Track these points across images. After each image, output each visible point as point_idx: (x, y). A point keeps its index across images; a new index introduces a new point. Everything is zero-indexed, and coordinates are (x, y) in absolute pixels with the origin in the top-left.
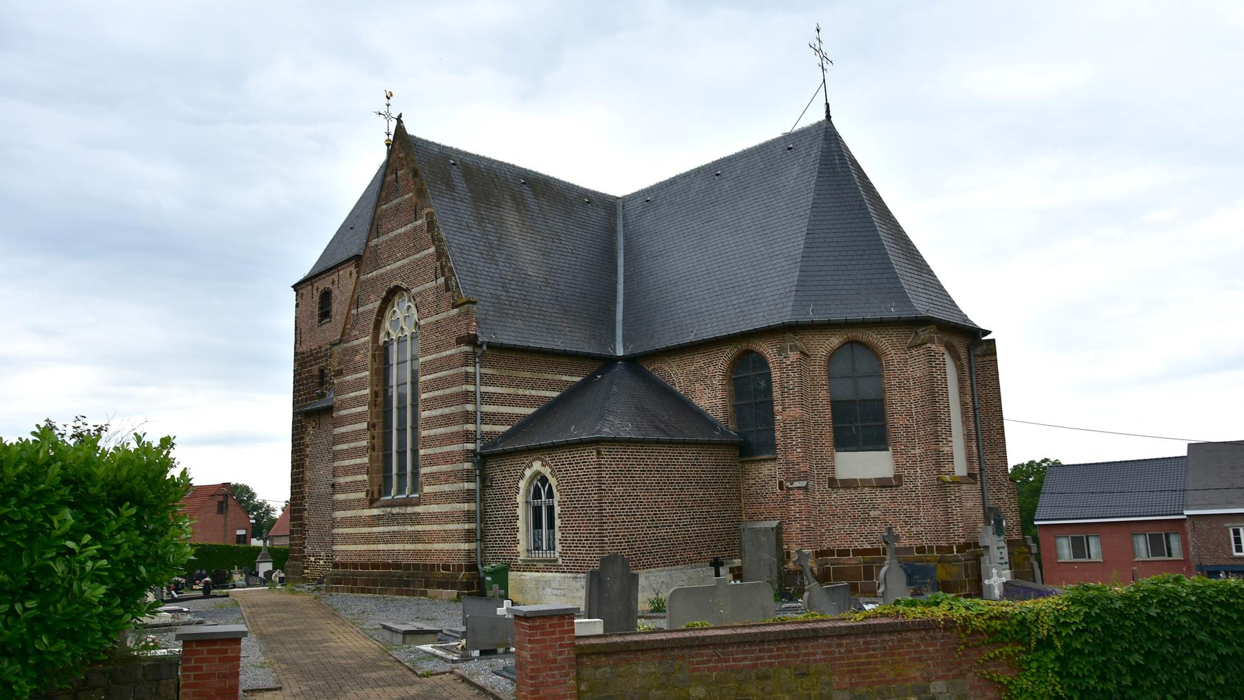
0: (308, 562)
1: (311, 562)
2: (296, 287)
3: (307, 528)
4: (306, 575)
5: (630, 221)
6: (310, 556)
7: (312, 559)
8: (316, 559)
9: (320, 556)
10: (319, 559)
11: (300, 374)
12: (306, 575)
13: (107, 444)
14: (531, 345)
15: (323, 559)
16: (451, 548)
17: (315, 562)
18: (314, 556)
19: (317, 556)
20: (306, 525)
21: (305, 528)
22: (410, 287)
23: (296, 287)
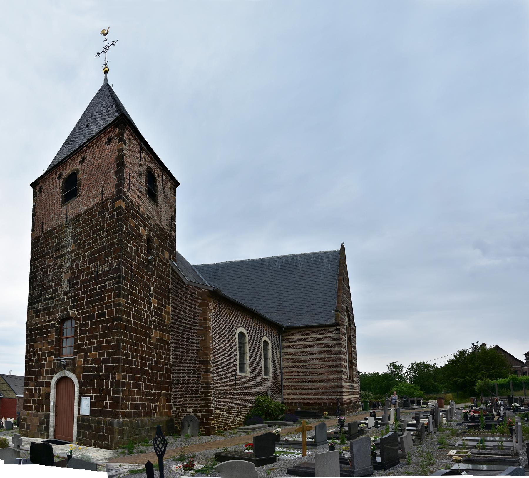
0: (214, 414)
1: (217, 414)
2: (33, 185)
3: (213, 387)
4: (213, 425)
5: (243, 421)
6: (216, 409)
7: (218, 412)
8: (220, 412)
9: (224, 409)
10: (223, 411)
11: (34, 268)
12: (213, 425)
13: (488, 347)
14: (100, 449)
15: (226, 411)
16: (288, 337)
17: (220, 414)
18: (218, 409)
19: (221, 409)
20: (211, 384)
21: (211, 387)
22: (454, 444)
23: (33, 185)
